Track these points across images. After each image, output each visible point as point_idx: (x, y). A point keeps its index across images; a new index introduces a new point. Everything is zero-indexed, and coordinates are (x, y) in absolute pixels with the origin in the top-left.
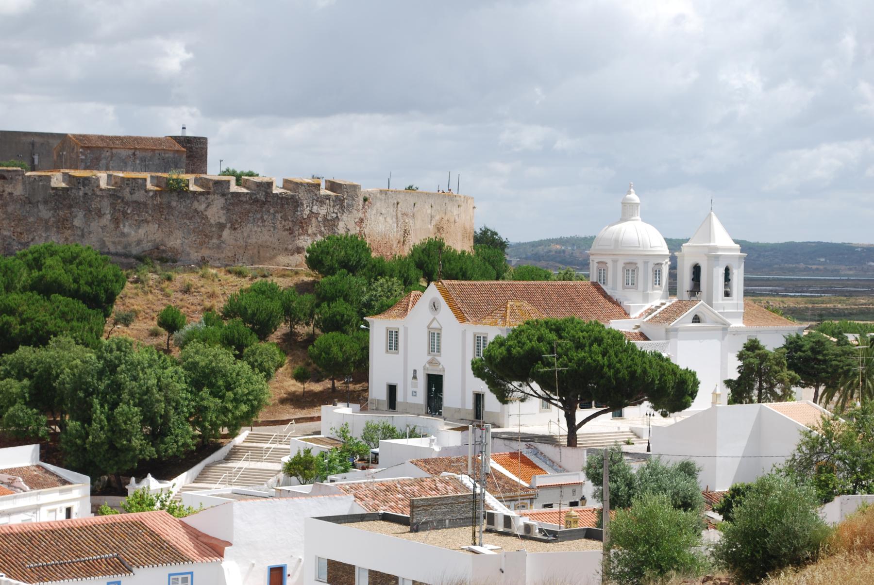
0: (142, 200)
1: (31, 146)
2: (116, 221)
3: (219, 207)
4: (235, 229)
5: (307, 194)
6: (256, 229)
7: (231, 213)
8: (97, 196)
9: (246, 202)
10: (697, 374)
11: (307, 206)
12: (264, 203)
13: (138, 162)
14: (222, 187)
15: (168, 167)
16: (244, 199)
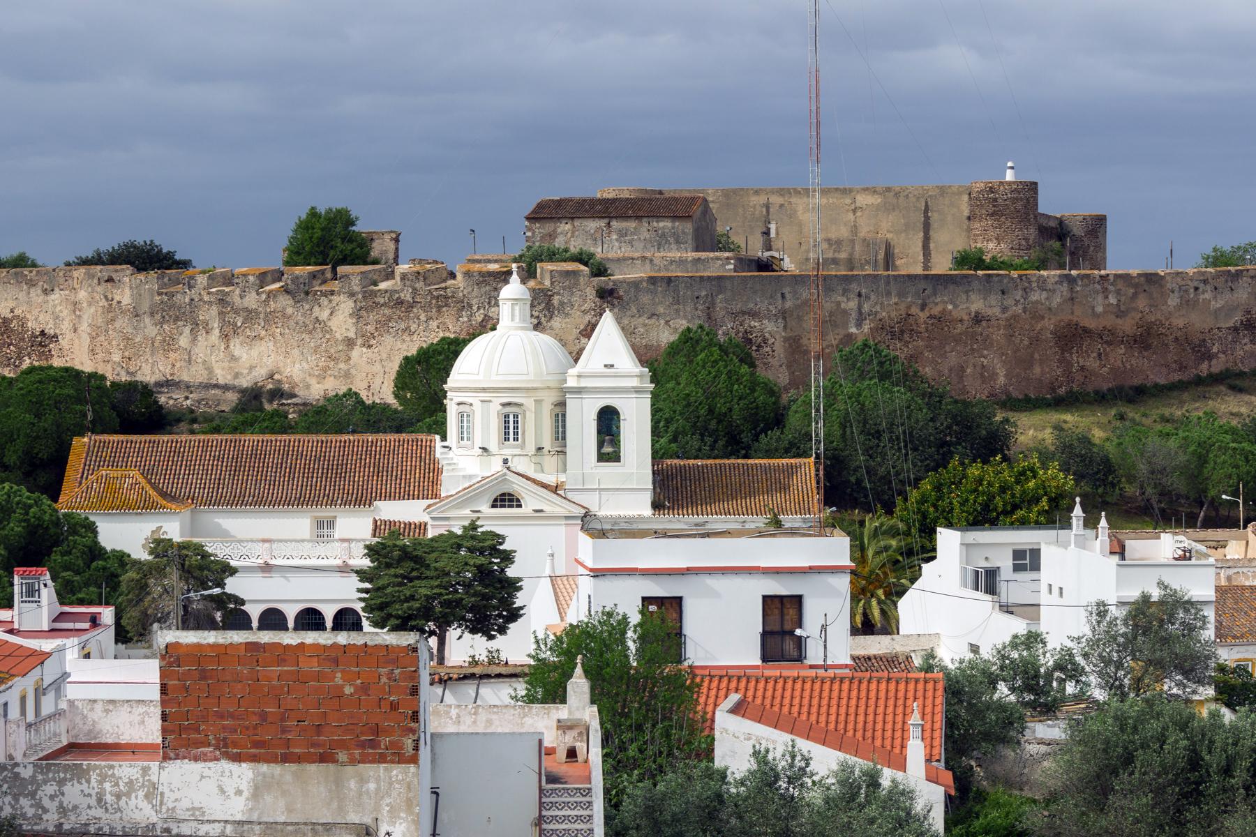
0: (253, 307)
1: (764, 210)
2: (225, 337)
3: (347, 314)
4: (370, 346)
5: (480, 288)
6: (401, 347)
7: (364, 323)
8: (205, 302)
9: (385, 304)
10: (1064, 550)
11: (479, 308)
12: (411, 306)
13: (615, 237)
14: (350, 283)
15: (664, 242)
16: (382, 301)
